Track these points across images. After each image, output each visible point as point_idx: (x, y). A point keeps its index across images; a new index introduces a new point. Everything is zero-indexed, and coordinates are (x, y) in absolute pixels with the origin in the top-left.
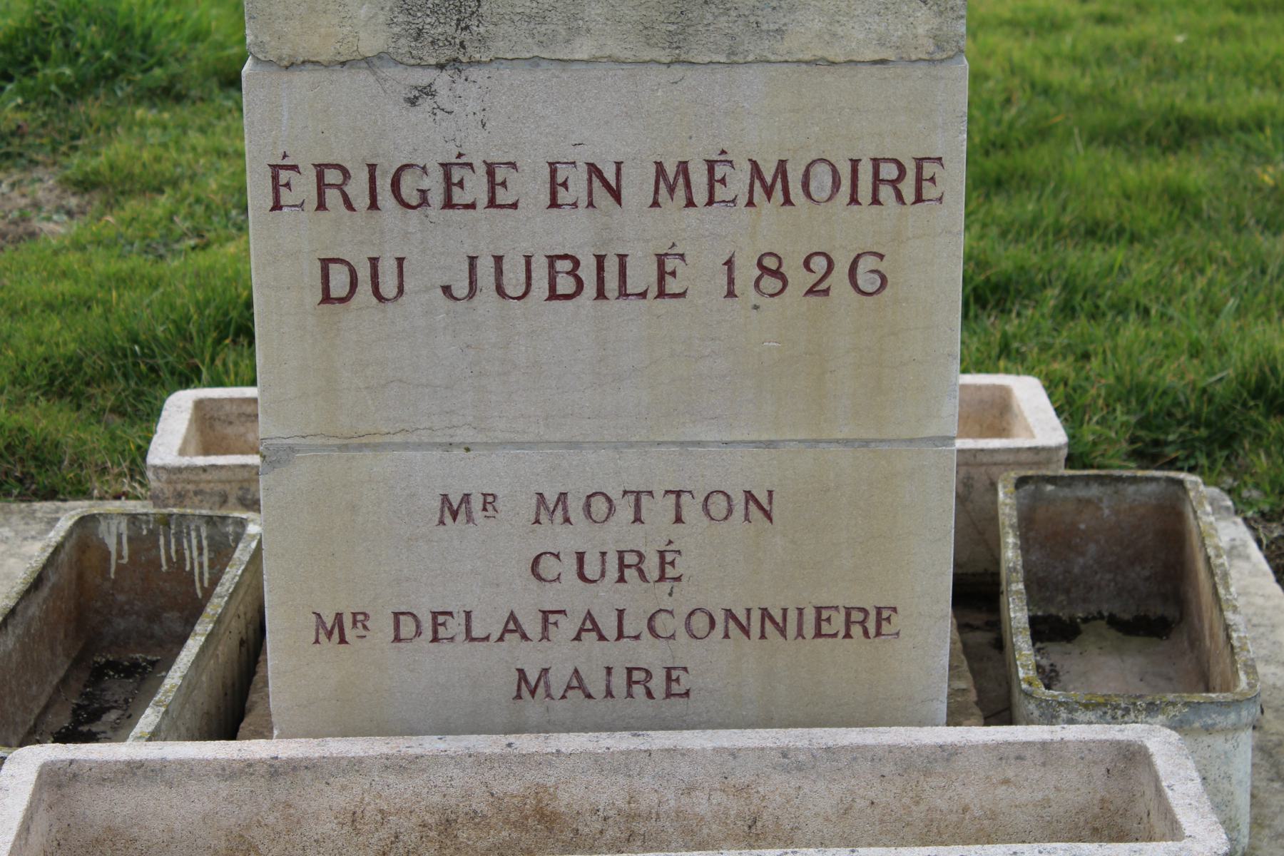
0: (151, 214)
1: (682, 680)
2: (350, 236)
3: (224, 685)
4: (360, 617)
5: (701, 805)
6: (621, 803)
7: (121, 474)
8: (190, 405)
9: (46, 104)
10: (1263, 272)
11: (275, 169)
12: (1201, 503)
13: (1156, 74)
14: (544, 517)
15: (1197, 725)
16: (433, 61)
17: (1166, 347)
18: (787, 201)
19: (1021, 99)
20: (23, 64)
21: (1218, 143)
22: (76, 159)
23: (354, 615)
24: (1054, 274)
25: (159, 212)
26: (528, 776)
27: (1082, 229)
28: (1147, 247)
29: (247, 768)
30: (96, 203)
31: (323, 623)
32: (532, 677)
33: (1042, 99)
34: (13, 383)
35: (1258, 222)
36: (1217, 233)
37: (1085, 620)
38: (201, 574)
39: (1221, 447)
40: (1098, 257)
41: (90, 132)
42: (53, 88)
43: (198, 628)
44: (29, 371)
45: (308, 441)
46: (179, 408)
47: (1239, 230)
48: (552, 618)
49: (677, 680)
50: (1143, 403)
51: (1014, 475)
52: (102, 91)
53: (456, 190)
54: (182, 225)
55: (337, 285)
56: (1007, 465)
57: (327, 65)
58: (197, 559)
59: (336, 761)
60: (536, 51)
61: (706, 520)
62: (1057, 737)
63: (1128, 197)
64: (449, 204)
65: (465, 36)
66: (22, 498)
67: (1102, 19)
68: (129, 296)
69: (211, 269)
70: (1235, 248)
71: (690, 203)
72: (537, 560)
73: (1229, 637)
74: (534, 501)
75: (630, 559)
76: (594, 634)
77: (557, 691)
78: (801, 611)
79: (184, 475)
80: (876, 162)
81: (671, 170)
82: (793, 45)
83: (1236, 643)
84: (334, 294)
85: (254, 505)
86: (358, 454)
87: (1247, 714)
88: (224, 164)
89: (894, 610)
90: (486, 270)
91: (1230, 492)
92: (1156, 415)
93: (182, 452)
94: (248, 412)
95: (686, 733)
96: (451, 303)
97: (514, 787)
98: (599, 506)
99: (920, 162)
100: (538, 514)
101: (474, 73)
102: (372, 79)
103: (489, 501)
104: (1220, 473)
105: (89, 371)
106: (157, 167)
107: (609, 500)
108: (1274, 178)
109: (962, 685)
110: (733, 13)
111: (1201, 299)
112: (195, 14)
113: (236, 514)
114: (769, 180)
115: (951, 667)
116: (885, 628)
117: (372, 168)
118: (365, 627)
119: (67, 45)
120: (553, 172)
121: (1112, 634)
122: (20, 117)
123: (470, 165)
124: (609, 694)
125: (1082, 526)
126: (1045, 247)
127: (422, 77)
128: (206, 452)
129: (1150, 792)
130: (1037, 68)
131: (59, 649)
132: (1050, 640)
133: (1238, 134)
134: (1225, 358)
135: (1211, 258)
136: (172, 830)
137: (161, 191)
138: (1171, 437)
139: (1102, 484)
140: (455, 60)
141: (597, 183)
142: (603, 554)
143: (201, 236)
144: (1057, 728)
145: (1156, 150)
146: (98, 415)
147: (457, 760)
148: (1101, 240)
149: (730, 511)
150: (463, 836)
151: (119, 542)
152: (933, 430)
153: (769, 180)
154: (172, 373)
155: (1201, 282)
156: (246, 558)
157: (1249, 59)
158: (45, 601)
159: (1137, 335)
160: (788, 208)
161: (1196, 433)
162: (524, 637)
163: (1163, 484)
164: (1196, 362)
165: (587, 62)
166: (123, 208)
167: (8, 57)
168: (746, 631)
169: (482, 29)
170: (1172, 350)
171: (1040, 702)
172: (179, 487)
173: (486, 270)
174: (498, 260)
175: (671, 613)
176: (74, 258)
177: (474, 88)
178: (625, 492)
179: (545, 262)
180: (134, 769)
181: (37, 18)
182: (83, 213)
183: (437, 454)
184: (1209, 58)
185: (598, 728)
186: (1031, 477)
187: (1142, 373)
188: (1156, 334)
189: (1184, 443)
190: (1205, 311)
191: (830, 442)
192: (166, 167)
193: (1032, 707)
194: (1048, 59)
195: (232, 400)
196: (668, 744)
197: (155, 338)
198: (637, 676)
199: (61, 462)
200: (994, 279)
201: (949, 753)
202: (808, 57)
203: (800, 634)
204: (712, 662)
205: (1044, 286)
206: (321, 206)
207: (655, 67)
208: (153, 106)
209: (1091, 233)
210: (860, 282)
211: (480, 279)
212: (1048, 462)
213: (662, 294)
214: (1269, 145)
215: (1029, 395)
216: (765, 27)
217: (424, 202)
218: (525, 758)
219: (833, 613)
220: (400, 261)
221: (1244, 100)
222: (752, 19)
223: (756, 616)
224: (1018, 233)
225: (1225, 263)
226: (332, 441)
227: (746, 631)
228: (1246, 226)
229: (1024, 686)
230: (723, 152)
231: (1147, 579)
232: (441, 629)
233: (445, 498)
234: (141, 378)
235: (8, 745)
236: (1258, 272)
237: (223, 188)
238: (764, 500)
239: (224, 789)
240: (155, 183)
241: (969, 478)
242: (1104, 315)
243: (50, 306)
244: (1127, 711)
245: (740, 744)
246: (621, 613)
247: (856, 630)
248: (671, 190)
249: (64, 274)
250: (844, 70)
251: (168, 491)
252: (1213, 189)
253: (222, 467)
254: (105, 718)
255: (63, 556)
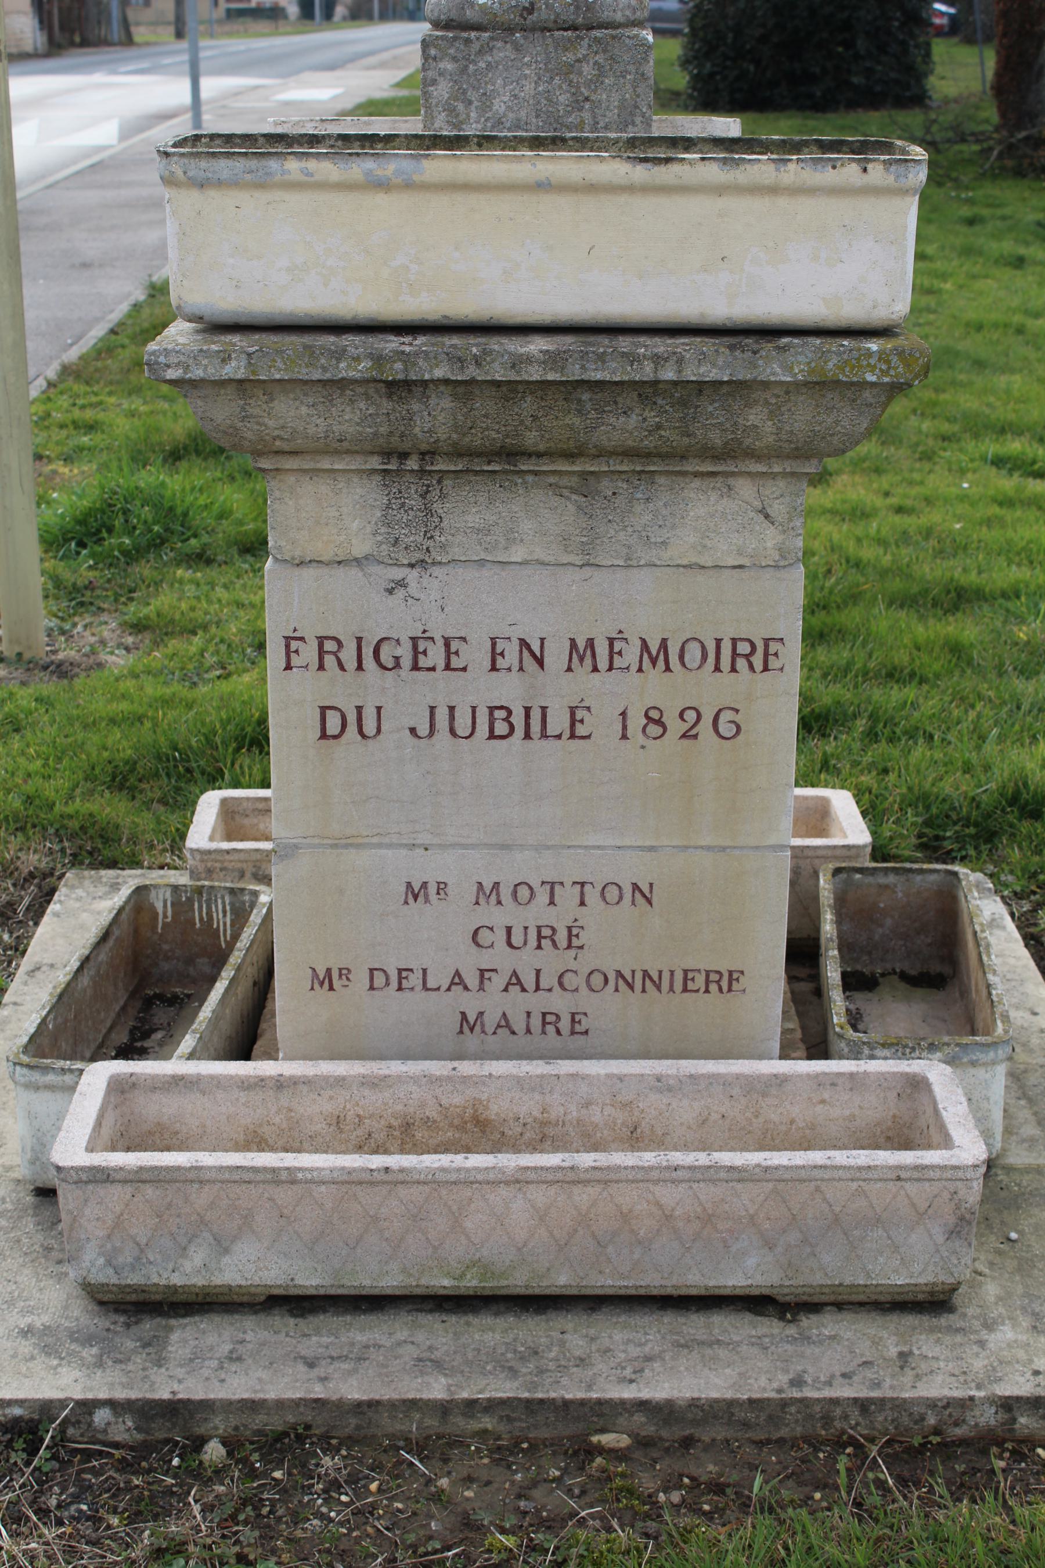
0: (187, 650)
1: (583, 1022)
2: (342, 690)
3: (242, 1016)
4: (344, 972)
5: (596, 1115)
6: (536, 1113)
7: (165, 850)
8: (217, 802)
9: (111, 565)
10: (1019, 708)
11: (288, 639)
12: (970, 890)
13: (939, 553)
14: (482, 900)
15: (965, 1060)
16: (406, 562)
17: (945, 765)
18: (668, 669)
19: (839, 570)
20: (95, 534)
21: (986, 607)
22: (132, 608)
23: (340, 970)
24: (863, 706)
25: (193, 649)
26: (468, 1092)
27: (884, 672)
28: (932, 687)
29: (260, 1083)
30: (147, 641)
31: (317, 976)
32: (471, 1019)
33: (854, 570)
34: (86, 780)
35: (1015, 669)
36: (984, 677)
37: (883, 975)
38: (225, 930)
39: (986, 842)
40: (895, 695)
41: (143, 587)
42: (116, 553)
43: (223, 974)
44: (97, 771)
45: (308, 841)
46: (209, 805)
47: (1000, 675)
48: (487, 975)
49: (579, 1022)
50: (928, 808)
51: (831, 866)
52: (152, 556)
53: (421, 657)
54: (210, 659)
55: (331, 727)
56: (826, 858)
57: (327, 564)
58: (222, 920)
59: (326, 1078)
60: (483, 555)
61: (603, 903)
62: (861, 1069)
63: (919, 649)
64: (415, 667)
65: (430, 543)
66: (92, 866)
67: (900, 510)
68: (171, 714)
69: (232, 694)
70: (997, 688)
71: (595, 669)
72: (476, 932)
73: (990, 994)
74: (475, 888)
75: (546, 932)
76: (518, 987)
77: (489, 1029)
78: (672, 973)
79: (213, 856)
80: (734, 641)
81: (581, 644)
82: (676, 553)
83: (995, 999)
84: (329, 732)
85: (266, 880)
86: (345, 851)
87: (1002, 1052)
88: (242, 613)
89: (742, 972)
90: (442, 715)
91: (991, 876)
92: (937, 817)
93: (211, 839)
94: (263, 808)
95: (586, 1062)
96: (416, 740)
97: (457, 1100)
98: (524, 893)
99: (767, 641)
100: (478, 898)
101: (436, 571)
102: (360, 574)
103: (442, 887)
104: (985, 862)
105: (142, 771)
106: (192, 615)
107: (531, 888)
108: (1027, 635)
109: (791, 1026)
110: (630, 529)
111: (971, 727)
112: (222, 498)
113: (251, 887)
114: (654, 653)
115: (784, 1012)
116: (735, 986)
117: (359, 640)
118: (348, 979)
119: (127, 521)
120: (494, 645)
121: (902, 985)
122: (91, 574)
123: (432, 639)
124: (528, 1031)
125: (882, 905)
126: (856, 687)
127: (398, 573)
128: (229, 838)
129: (930, 1111)
130: (851, 547)
131: (121, 984)
132: (856, 989)
133: (1001, 601)
134: (989, 774)
135: (980, 697)
136: (204, 1126)
137: (194, 633)
138: (948, 834)
139: (897, 874)
140: (422, 561)
141: (526, 653)
142: (526, 928)
143: (224, 668)
144: (862, 1062)
145: (940, 612)
146: (148, 805)
147: (415, 1079)
148: (897, 681)
149: (621, 898)
150: (419, 1135)
151: (165, 906)
152: (772, 840)
153: (654, 653)
154: (203, 773)
155: (972, 715)
156: (259, 921)
157: (1009, 542)
158: (111, 950)
159: (924, 756)
160: (668, 674)
161: (967, 831)
162: (466, 988)
163: (942, 875)
164: (967, 776)
165: (520, 564)
166: (166, 646)
167: (83, 529)
168: (631, 987)
169: (443, 539)
170: (950, 767)
171: (849, 1042)
172: (209, 865)
173: (442, 715)
174: (452, 709)
175: (575, 972)
176: (130, 684)
177: (436, 582)
178: (543, 883)
179: (487, 711)
180: (177, 1081)
181: (105, 501)
182: (137, 649)
183: (404, 852)
184: (980, 541)
185: (520, 1057)
186: (844, 868)
187: (927, 785)
188: (938, 755)
189: (958, 838)
190: (975, 737)
191: (696, 848)
192: (199, 615)
193: (843, 1045)
194: (859, 540)
195: (248, 799)
196: (572, 1070)
197: (190, 747)
198: (550, 1018)
199: (120, 840)
200: (817, 710)
201: (781, 1080)
202: (685, 562)
203: (671, 989)
204: (605, 1009)
205: (855, 716)
206: (321, 667)
207: (571, 568)
208: (190, 567)
209: (890, 675)
210: (721, 730)
211: (437, 724)
212: (857, 856)
213: (573, 736)
214: (1024, 609)
215: (842, 802)
216: (653, 540)
217: (397, 665)
218: (465, 1079)
219: (696, 974)
220: (379, 709)
221: (1007, 574)
222: (644, 534)
223: (639, 976)
224: (836, 676)
225: (990, 700)
226: (325, 841)
227: (631, 987)
228: (1006, 672)
229: (837, 1029)
230: (620, 632)
231: (930, 945)
232: (404, 981)
233: (409, 885)
234: (179, 777)
235: (83, 1059)
236: (1014, 708)
237: (241, 631)
238: (646, 890)
239: (243, 1096)
240: (190, 627)
241: (798, 867)
242: (899, 739)
243: (113, 721)
244: (913, 1049)
245: (625, 1071)
246: (538, 972)
247: (713, 987)
248: (581, 659)
249: (123, 696)
250: (711, 572)
251: (201, 868)
252: (982, 642)
253: (241, 851)
254: (153, 1036)
255: (124, 916)
